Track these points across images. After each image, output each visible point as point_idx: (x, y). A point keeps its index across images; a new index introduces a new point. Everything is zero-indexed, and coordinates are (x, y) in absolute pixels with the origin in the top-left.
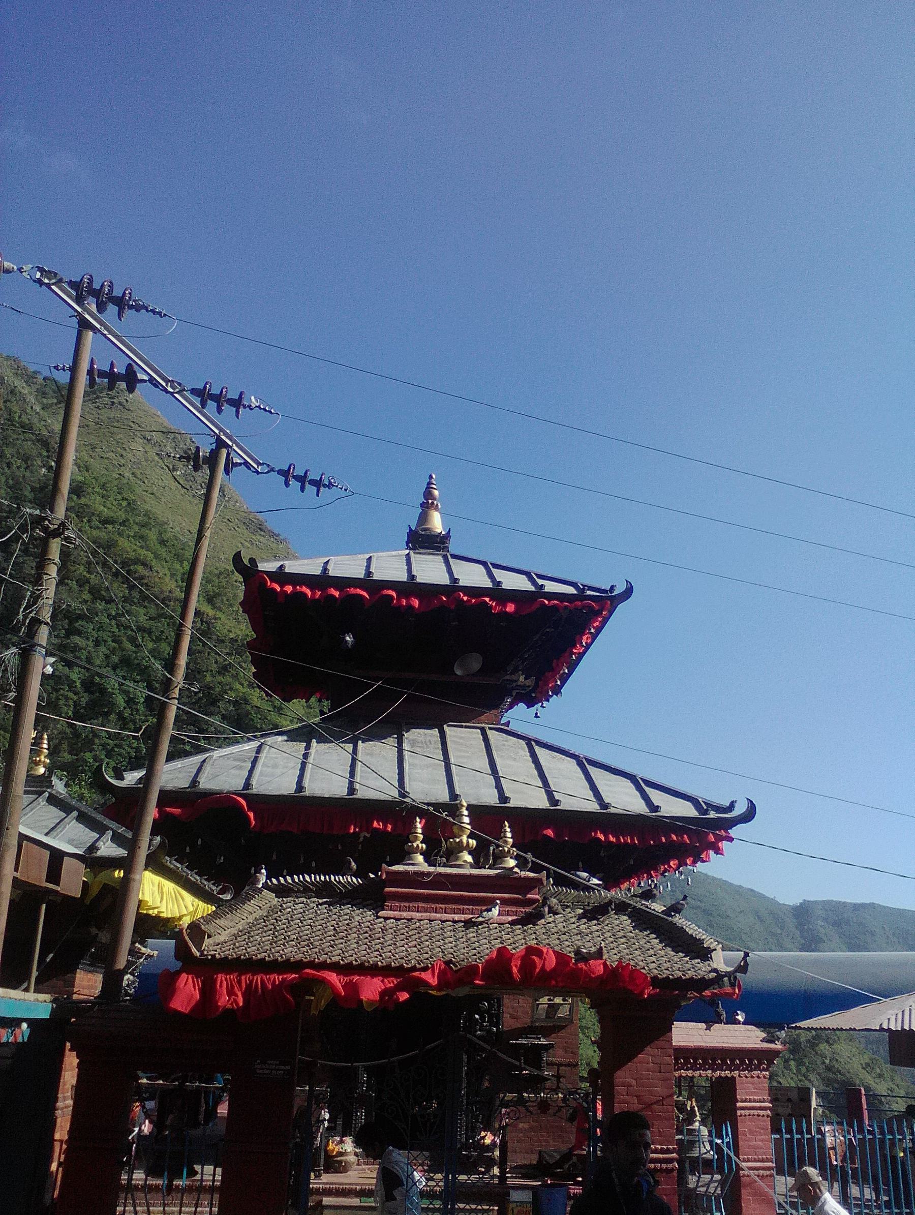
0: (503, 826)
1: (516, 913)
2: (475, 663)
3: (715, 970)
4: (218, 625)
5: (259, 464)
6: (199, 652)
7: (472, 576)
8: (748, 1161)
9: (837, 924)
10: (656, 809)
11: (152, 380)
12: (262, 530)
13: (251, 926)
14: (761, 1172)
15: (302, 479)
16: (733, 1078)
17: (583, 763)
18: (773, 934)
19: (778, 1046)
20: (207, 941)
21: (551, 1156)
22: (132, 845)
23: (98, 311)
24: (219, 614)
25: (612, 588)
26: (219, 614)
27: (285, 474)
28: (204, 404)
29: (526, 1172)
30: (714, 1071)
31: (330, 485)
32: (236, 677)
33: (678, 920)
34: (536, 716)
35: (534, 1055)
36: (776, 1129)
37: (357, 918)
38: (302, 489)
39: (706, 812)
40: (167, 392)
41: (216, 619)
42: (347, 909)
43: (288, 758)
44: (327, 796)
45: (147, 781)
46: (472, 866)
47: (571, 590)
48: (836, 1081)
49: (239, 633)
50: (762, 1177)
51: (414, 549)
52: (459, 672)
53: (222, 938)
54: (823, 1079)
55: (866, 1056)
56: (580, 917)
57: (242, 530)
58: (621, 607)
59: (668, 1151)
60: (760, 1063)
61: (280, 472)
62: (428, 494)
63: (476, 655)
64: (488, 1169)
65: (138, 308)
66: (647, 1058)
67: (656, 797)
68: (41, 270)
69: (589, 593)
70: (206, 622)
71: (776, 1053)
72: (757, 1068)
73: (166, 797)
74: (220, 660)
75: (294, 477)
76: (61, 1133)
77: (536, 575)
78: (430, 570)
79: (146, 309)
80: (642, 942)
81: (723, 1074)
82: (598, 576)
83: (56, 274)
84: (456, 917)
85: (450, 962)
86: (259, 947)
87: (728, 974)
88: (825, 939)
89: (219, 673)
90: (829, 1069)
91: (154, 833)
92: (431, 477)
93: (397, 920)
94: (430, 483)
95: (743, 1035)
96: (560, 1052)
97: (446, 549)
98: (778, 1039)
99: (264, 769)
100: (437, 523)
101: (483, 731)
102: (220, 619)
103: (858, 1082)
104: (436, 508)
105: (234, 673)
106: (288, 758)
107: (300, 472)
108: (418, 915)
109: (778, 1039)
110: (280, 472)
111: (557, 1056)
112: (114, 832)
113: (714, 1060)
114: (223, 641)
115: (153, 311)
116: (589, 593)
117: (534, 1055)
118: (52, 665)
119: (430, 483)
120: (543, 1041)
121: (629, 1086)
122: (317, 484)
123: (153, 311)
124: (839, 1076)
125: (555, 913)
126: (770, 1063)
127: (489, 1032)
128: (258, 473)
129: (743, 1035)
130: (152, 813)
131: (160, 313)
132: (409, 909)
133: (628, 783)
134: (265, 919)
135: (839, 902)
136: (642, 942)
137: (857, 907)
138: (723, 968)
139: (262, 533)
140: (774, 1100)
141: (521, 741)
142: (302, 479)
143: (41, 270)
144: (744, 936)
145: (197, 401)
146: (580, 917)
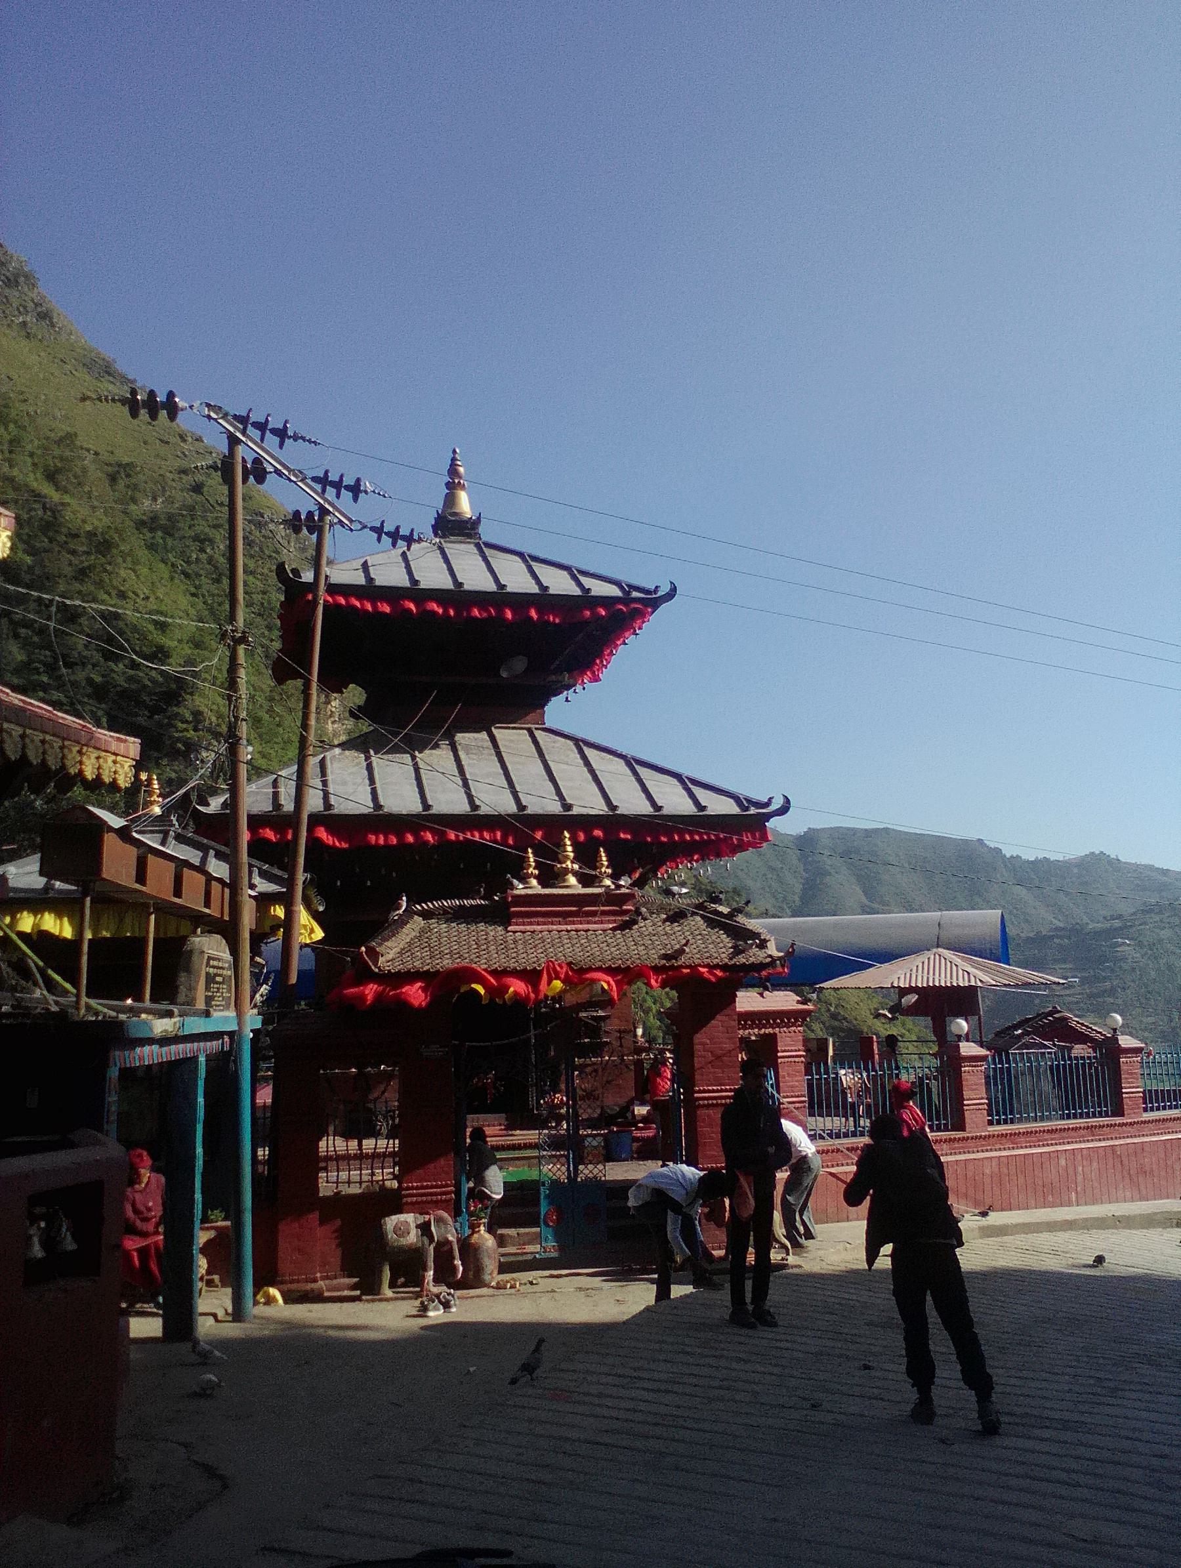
0: (599, 852)
1: (615, 921)
2: (520, 664)
3: (770, 956)
4: (68, 515)
5: (351, 521)
6: (46, 551)
7: (517, 579)
8: (787, 1097)
9: (846, 854)
10: (703, 808)
11: (277, 471)
12: (109, 374)
13: (410, 944)
14: (797, 1105)
16: (775, 1034)
17: (632, 763)
18: (773, 869)
19: (810, 1007)
20: (381, 959)
21: (612, 1109)
22: (290, 883)
24: (67, 499)
26: (67, 499)
27: (379, 531)
28: (324, 491)
29: (593, 1124)
30: (760, 1029)
32: (100, 584)
33: (741, 919)
34: (567, 700)
35: (594, 1028)
36: (808, 1071)
37: (492, 933)
39: (747, 809)
40: (290, 480)
41: (63, 504)
42: (482, 926)
44: (404, 812)
45: (233, 804)
47: (615, 591)
48: (842, 1030)
49: (96, 523)
50: (797, 1108)
51: (444, 536)
52: (504, 674)
53: (390, 957)
54: (827, 1029)
55: (875, 1000)
56: (664, 921)
57: (83, 374)
59: (447, 1186)
60: (797, 1020)
61: (373, 529)
62: (453, 471)
63: (525, 660)
64: (559, 1124)
65: (296, 438)
66: (717, 1024)
67: (702, 795)
68: (208, 405)
69: (635, 594)
70: (51, 510)
71: (808, 1012)
72: (794, 1025)
73: (256, 821)
74: (75, 561)
75: (386, 534)
76: (15, 1139)
78: (474, 576)
79: (303, 439)
80: (714, 937)
81: (767, 1031)
82: (647, 577)
83: (220, 408)
84: (569, 928)
85: (571, 963)
86: (420, 961)
87: (780, 958)
88: (832, 871)
89: (76, 579)
90: (834, 1016)
91: (305, 871)
92: (454, 452)
93: (524, 932)
94: (454, 459)
95: (783, 1000)
96: (616, 1021)
98: (810, 1000)
100: (465, 505)
101: (530, 731)
102: (69, 504)
103: (865, 1030)
104: (463, 487)
105: (97, 579)
108: (539, 928)
109: (810, 1000)
110: (373, 529)
111: (612, 1026)
112: (259, 869)
113: (760, 1021)
114: (76, 536)
115: (310, 441)
116: (635, 594)
117: (594, 1028)
118: (251, 753)
119: (454, 459)
120: (601, 1013)
121: (704, 1044)
123: (310, 441)
124: (845, 1024)
125: (645, 919)
126: (804, 1019)
127: (554, 1008)
128: (351, 530)
129: (783, 1000)
130: (245, 836)
131: (315, 443)
132: (531, 924)
133: (675, 781)
134: (419, 938)
135: (848, 829)
136: (714, 937)
137: (868, 833)
138: (776, 954)
139: (111, 379)
140: (807, 1051)
141: (568, 742)
143: (208, 405)
144: (740, 873)
145: (318, 487)
146: (664, 921)
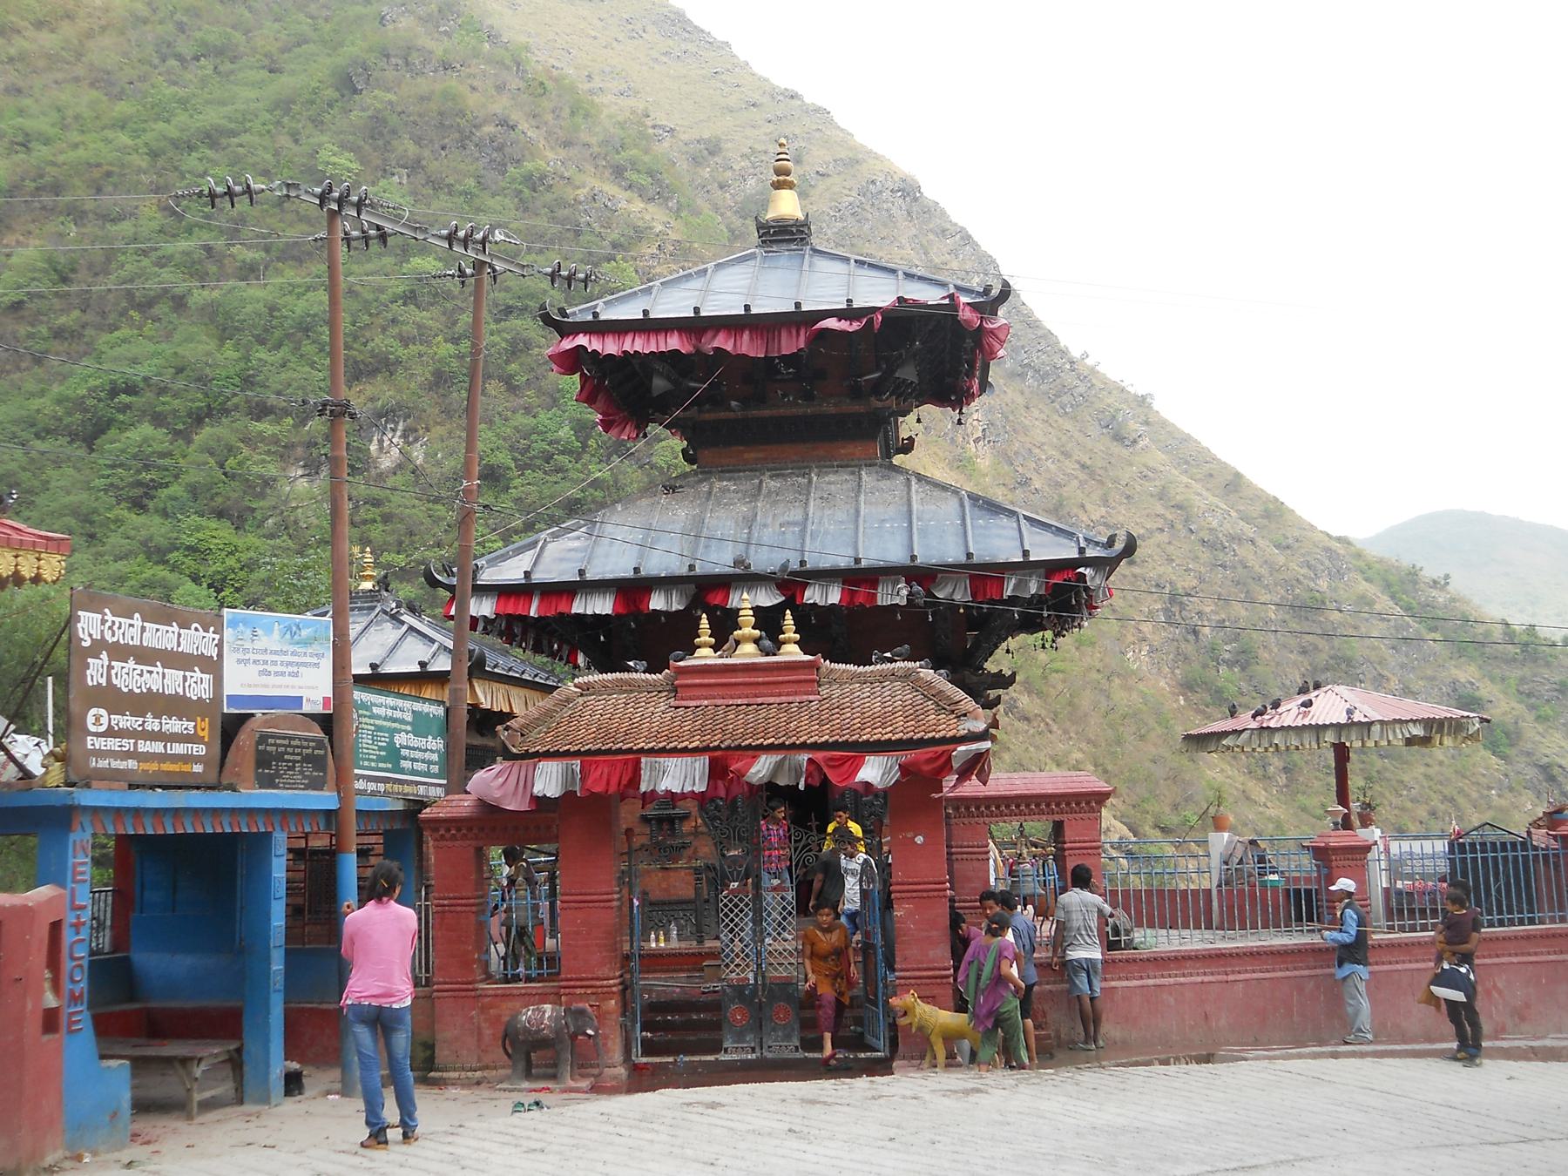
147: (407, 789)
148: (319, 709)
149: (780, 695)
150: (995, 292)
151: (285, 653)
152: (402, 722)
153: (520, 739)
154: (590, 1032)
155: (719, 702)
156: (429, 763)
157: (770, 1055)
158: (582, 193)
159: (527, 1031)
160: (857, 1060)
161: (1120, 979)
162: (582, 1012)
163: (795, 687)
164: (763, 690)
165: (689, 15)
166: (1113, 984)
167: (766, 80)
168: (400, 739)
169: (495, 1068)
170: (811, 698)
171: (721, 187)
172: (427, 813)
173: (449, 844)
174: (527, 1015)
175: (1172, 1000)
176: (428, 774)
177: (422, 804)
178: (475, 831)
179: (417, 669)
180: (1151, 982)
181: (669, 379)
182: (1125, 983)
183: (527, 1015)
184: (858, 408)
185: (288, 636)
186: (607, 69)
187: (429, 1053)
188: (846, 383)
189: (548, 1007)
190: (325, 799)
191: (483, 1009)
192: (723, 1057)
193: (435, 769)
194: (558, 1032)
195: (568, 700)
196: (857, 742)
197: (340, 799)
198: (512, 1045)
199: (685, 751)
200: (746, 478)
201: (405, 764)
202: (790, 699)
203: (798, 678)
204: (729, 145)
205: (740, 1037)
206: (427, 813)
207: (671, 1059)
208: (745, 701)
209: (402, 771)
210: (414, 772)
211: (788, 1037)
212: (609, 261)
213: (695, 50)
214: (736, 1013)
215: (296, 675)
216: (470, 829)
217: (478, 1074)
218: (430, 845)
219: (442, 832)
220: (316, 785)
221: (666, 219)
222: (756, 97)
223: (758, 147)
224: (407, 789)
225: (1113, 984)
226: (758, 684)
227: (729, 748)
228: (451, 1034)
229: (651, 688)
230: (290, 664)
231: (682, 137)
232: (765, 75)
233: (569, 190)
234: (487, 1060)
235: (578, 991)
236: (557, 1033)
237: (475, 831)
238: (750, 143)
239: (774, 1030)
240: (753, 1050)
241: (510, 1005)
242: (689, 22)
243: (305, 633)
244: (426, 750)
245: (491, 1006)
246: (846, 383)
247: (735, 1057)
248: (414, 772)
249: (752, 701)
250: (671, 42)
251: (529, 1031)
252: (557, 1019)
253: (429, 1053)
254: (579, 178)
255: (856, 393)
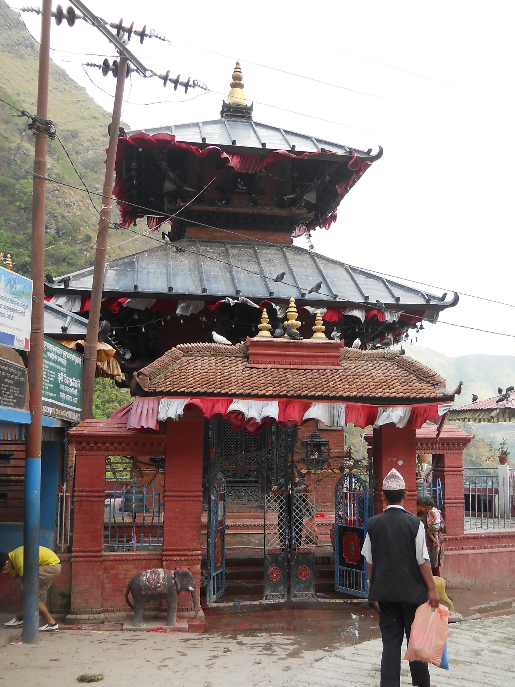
15: (176, 82)
23: (78, 343)
25: (370, 150)
31: (194, 86)
38: (175, 88)
43: (76, 166)
46: (453, 632)
58: (375, 164)
67: (398, 293)
77: (316, 139)
97: (250, 118)
99: (151, 495)
106: (76, 166)
107: (173, 76)
110: (160, 77)
122: (186, 85)
142: (176, 82)
147: (63, 413)
148: (22, 347)
149: (317, 364)
150: (374, 153)
151: (6, 299)
152: (61, 365)
153: (149, 382)
154: (191, 588)
155: (278, 366)
156: (73, 395)
157: (294, 600)
158: (13, 145)
159: (147, 588)
160: (352, 604)
161: (470, 549)
162: (186, 575)
163: (326, 360)
164: (306, 360)
165: (68, 72)
166: (467, 551)
167: (101, 107)
168: (61, 377)
169: (113, 611)
170: (337, 368)
171: (77, 153)
172: (74, 430)
173: (89, 453)
174: (146, 576)
175: (496, 561)
176: (72, 404)
177: (68, 424)
178: (132, 445)
179: (60, 332)
180: (486, 551)
181: (175, 183)
182: (473, 551)
183: (146, 576)
184: (283, 212)
185: (9, 287)
186: (27, 92)
187: (65, 601)
188: (275, 199)
189: (161, 570)
190: (21, 416)
191: (106, 570)
192: (265, 602)
193: (76, 400)
194: (170, 589)
195: (177, 358)
196: (381, 397)
197: (32, 416)
198: (134, 597)
199: (264, 397)
200: (217, 246)
201: (62, 395)
202: (324, 367)
203: (328, 354)
204: (82, 134)
205: (275, 588)
206: (74, 430)
207: (231, 604)
208: (295, 367)
209: (59, 399)
210: (66, 402)
211: (307, 588)
212: (24, 178)
213: (69, 89)
214: (273, 572)
215: (11, 318)
216: (128, 444)
217: (102, 616)
218: (73, 451)
219: (84, 444)
220: (19, 404)
221: (52, 163)
222: (96, 114)
223: (96, 137)
224: (63, 413)
225: (467, 551)
226: (303, 356)
227: (292, 396)
228: (82, 589)
229: (230, 354)
230: (9, 309)
231: (60, 127)
232: (101, 105)
233: (7, 143)
234: (108, 605)
235: (175, 558)
236: (169, 589)
237: (132, 445)
238: (92, 135)
239: (298, 583)
240: (283, 596)
241: (125, 567)
242: (68, 76)
243: (19, 287)
244: (71, 387)
245: (112, 568)
246: (275, 199)
247: (272, 601)
248: (66, 402)
249: (300, 367)
250: (58, 84)
251: (149, 588)
252: (169, 579)
253: (65, 601)
254: (12, 139)
255: (281, 205)
